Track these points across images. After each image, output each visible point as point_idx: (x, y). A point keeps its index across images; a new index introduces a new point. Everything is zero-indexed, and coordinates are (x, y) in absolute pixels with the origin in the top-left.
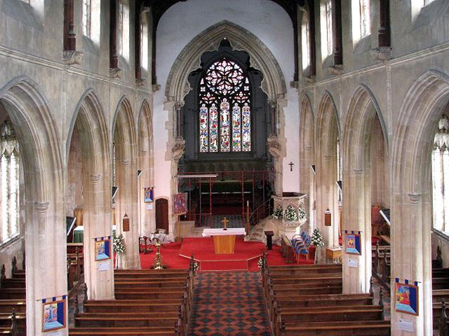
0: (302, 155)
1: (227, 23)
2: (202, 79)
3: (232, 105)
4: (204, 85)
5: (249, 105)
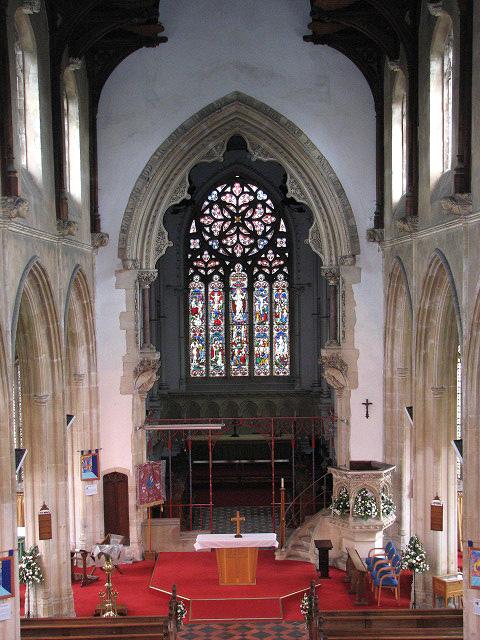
0: (388, 385)
1: (240, 99)
2: (194, 224)
3: (252, 279)
5: (288, 278)
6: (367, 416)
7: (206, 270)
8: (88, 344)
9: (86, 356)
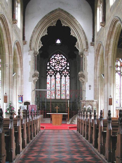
0: (95, 81)
1: (60, 10)
2: (48, 63)
3: (61, 76)
4: (49, 66)
5: (69, 76)
6: (90, 89)
7: (51, 74)
8: (21, 68)
9: (20, 71)
